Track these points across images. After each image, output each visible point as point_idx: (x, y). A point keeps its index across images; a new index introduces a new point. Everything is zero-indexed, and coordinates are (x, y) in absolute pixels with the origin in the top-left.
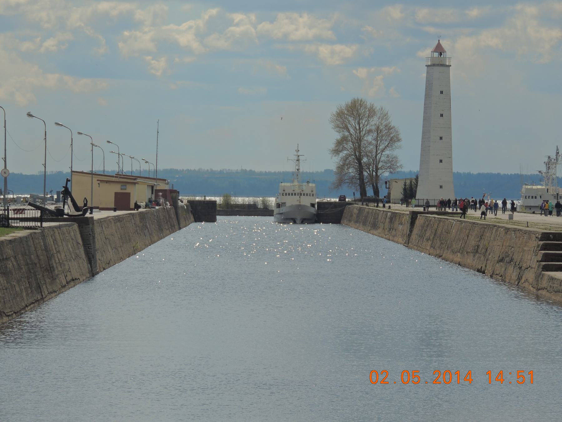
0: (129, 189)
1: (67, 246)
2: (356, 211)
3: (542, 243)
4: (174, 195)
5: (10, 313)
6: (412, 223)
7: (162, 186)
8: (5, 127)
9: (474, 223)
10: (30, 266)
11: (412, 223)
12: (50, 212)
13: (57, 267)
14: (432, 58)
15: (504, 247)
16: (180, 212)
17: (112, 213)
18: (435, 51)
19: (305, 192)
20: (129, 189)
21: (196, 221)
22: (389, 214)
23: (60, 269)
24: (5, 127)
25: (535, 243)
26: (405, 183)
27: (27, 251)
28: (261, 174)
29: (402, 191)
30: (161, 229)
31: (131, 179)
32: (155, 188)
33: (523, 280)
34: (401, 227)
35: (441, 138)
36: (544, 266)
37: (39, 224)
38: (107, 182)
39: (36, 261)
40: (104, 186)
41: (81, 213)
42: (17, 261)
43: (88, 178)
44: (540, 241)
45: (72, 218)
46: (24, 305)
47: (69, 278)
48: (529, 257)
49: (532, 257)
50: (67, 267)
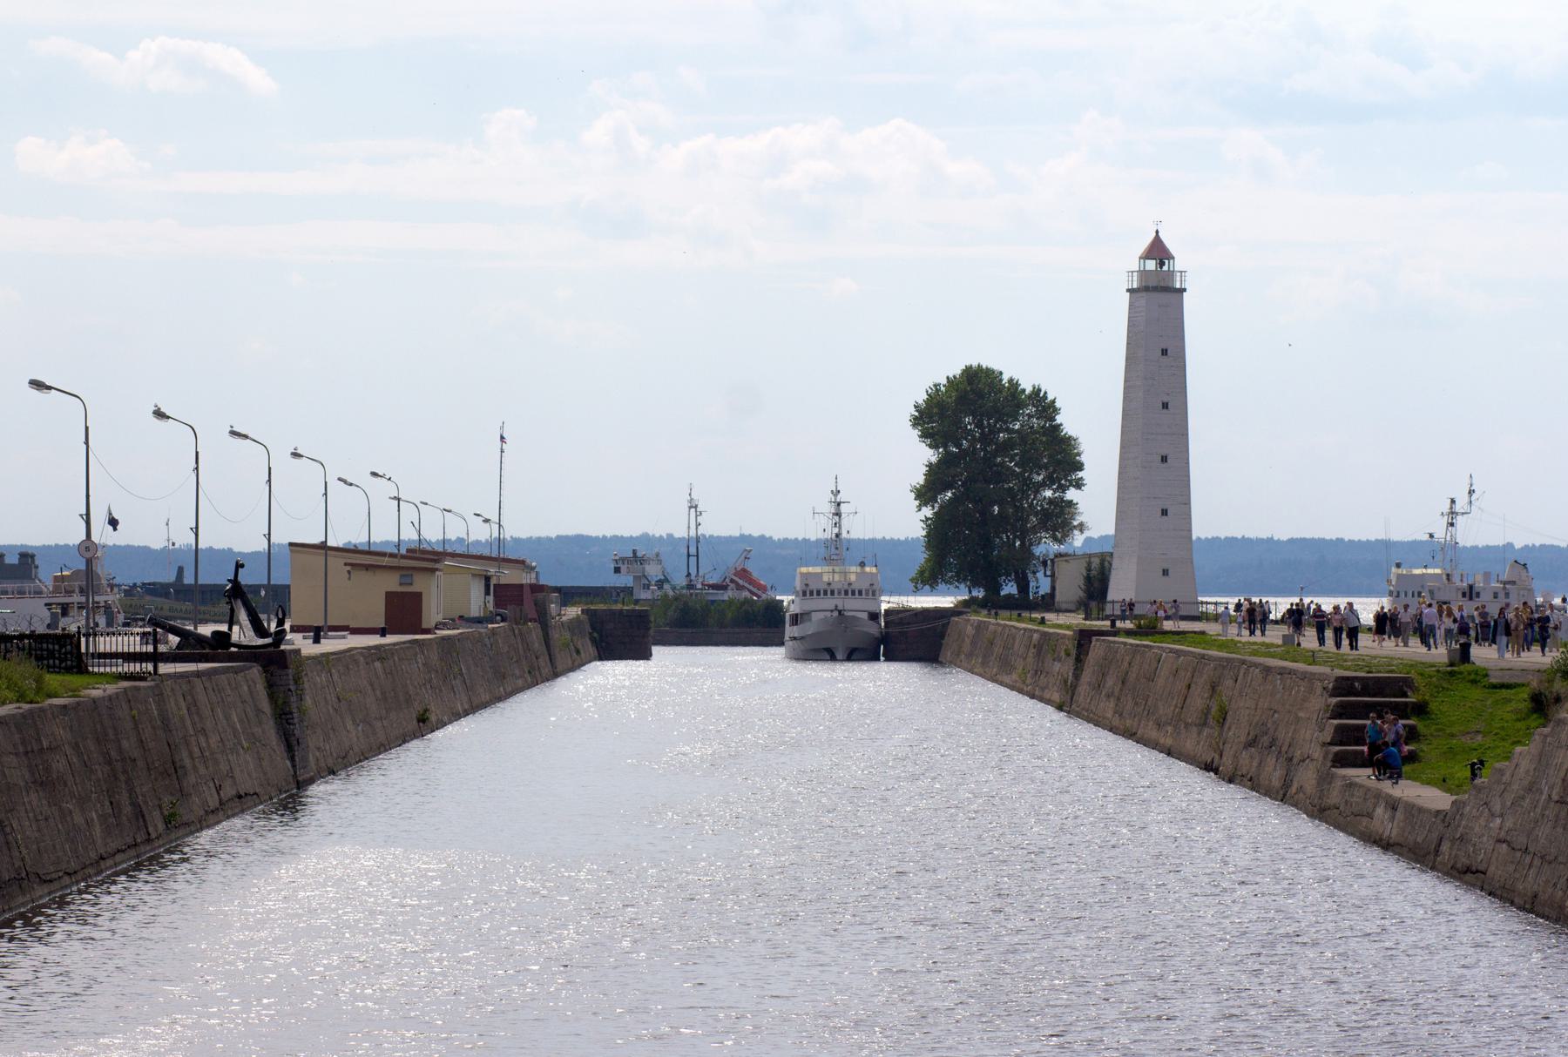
0: (419, 584)
1: (228, 718)
2: (970, 630)
3: (1334, 700)
4: (540, 596)
5: (55, 876)
6: (1079, 661)
7: (509, 576)
8: (87, 443)
9: (1203, 657)
10: (119, 766)
11: (1079, 661)
12: (201, 640)
13: (195, 767)
14: (1143, 274)
15: (1259, 712)
16: (555, 635)
17: (374, 640)
18: (1147, 255)
19: (856, 587)
20: (419, 584)
21: (601, 659)
22: (1036, 636)
23: (202, 770)
24: (87, 443)
25: (1321, 702)
26: (1089, 564)
27: (110, 732)
28: (785, 543)
29: (1081, 582)
30: (501, 677)
31: (1090, 556)
32: (493, 581)
33: (1294, 790)
34: (1057, 666)
35: (1164, 459)
36: (1336, 754)
37: (150, 667)
38: (367, 567)
39: (136, 754)
40: (362, 577)
41: (269, 640)
42: (80, 755)
43: (319, 559)
44: (1332, 695)
45: (248, 654)
46: (93, 855)
47: (229, 791)
48: (1308, 736)
49: (1312, 733)
50: (224, 768)
